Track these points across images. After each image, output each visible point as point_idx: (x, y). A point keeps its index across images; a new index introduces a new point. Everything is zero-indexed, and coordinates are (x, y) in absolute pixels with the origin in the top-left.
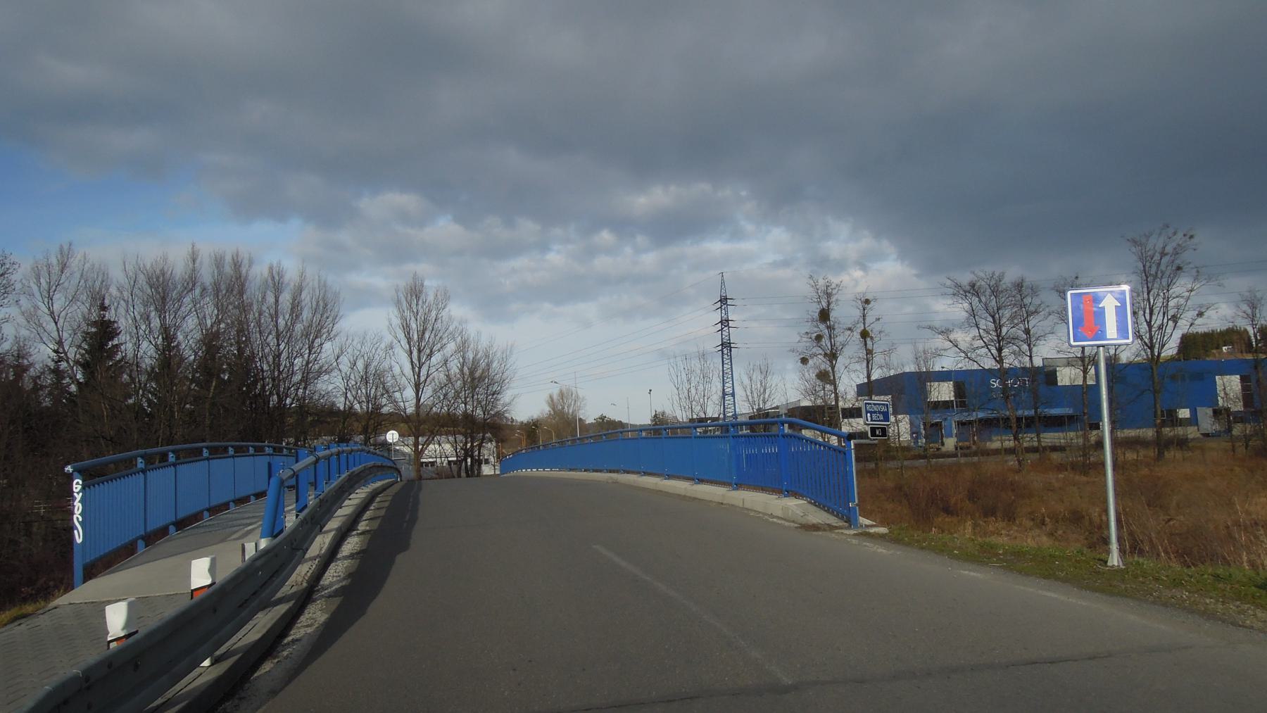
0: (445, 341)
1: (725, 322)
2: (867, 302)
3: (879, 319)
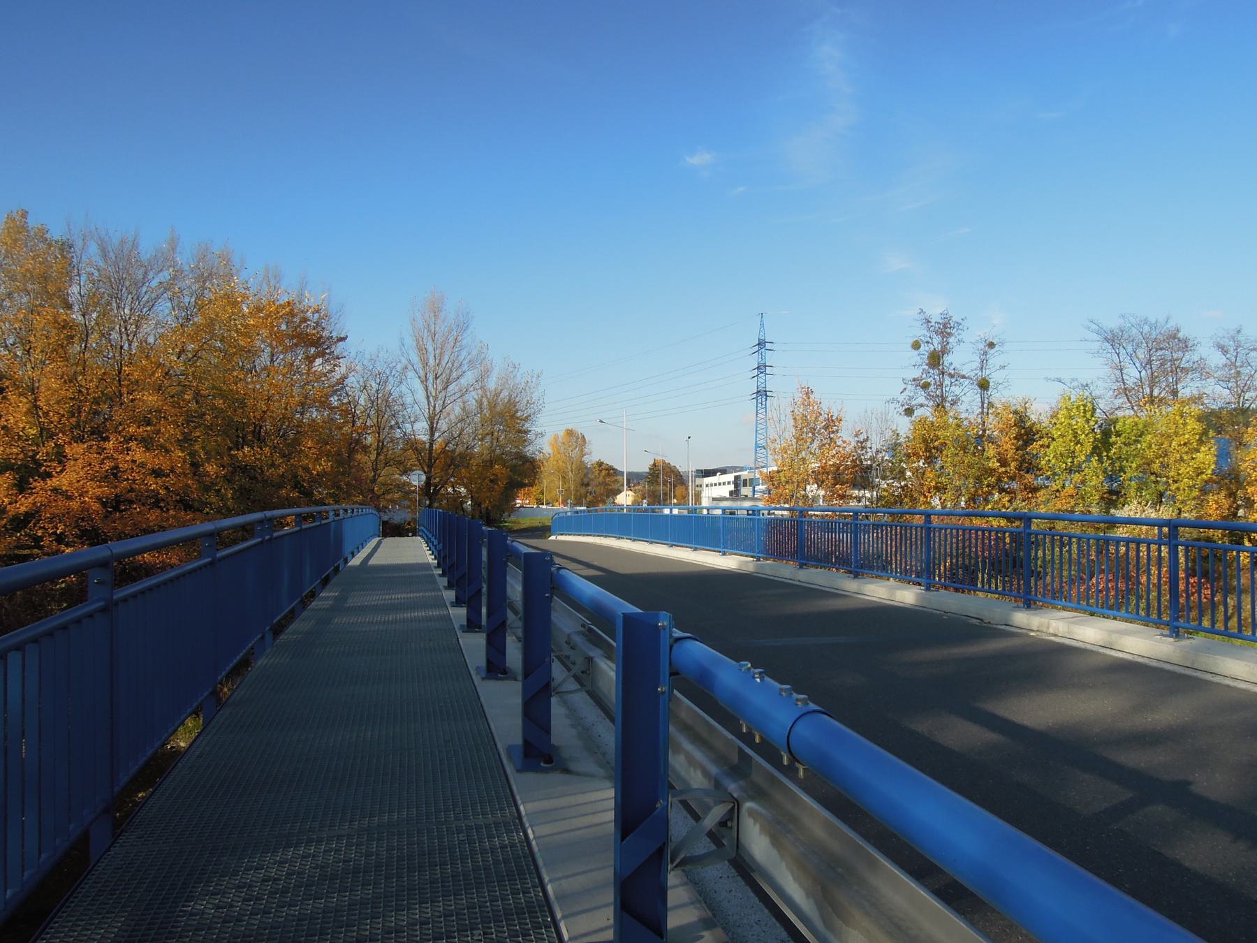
0: (465, 367)
1: (761, 368)
2: (991, 345)
3: (1004, 367)
